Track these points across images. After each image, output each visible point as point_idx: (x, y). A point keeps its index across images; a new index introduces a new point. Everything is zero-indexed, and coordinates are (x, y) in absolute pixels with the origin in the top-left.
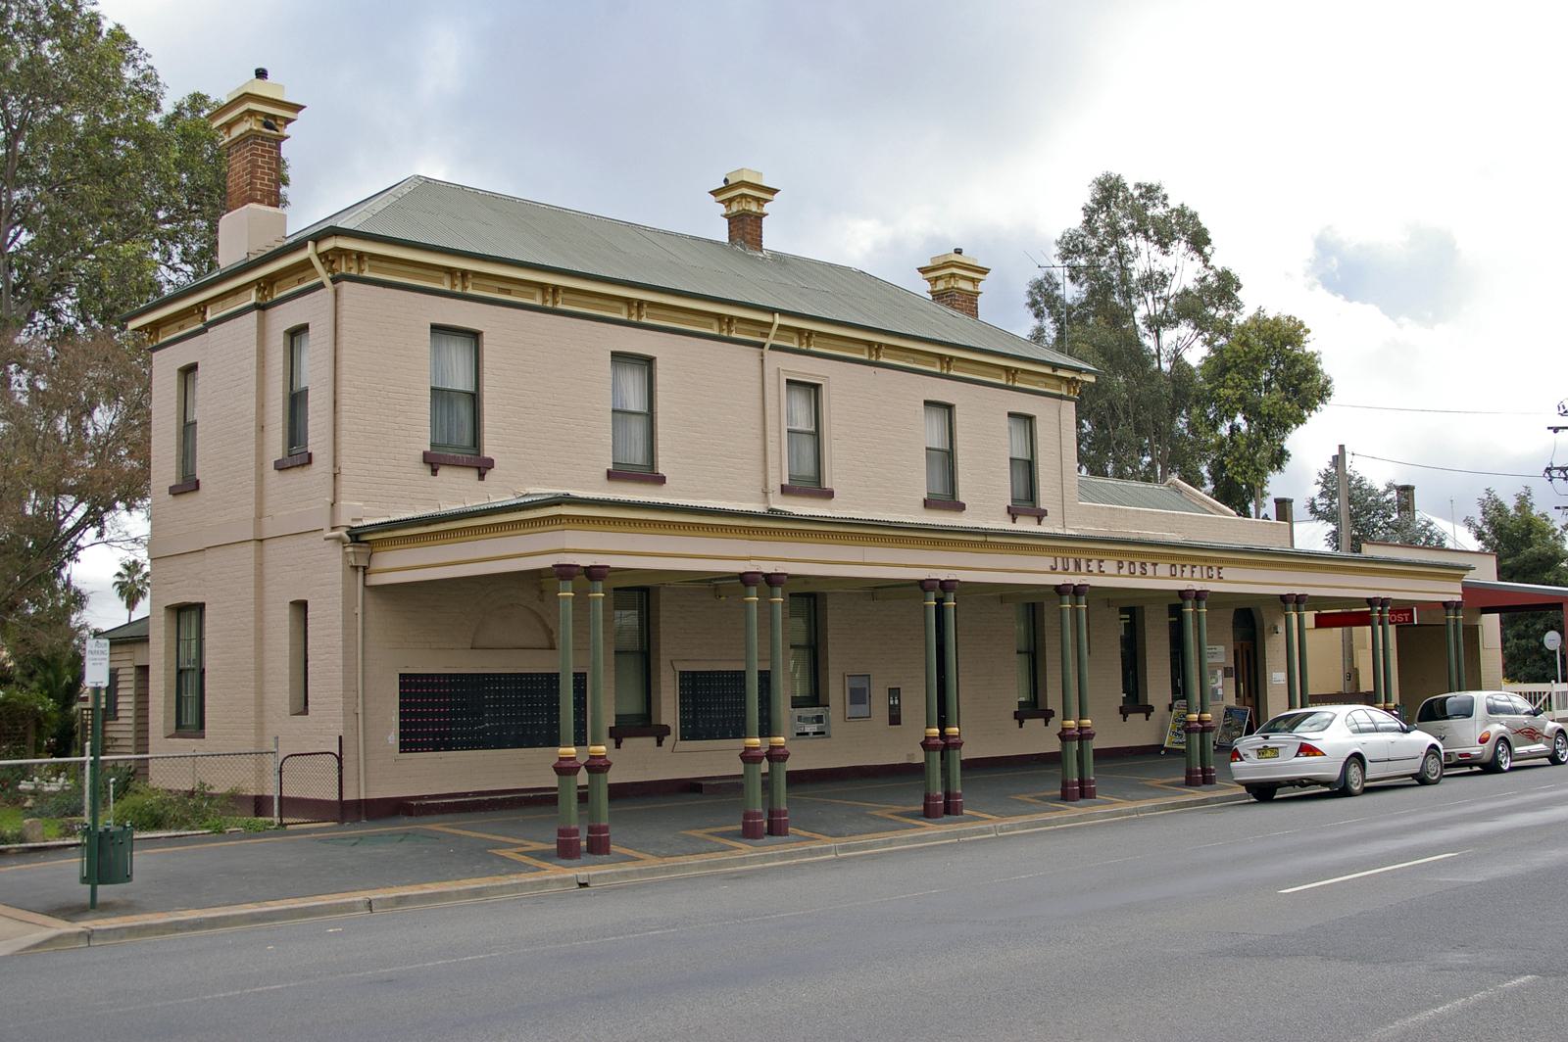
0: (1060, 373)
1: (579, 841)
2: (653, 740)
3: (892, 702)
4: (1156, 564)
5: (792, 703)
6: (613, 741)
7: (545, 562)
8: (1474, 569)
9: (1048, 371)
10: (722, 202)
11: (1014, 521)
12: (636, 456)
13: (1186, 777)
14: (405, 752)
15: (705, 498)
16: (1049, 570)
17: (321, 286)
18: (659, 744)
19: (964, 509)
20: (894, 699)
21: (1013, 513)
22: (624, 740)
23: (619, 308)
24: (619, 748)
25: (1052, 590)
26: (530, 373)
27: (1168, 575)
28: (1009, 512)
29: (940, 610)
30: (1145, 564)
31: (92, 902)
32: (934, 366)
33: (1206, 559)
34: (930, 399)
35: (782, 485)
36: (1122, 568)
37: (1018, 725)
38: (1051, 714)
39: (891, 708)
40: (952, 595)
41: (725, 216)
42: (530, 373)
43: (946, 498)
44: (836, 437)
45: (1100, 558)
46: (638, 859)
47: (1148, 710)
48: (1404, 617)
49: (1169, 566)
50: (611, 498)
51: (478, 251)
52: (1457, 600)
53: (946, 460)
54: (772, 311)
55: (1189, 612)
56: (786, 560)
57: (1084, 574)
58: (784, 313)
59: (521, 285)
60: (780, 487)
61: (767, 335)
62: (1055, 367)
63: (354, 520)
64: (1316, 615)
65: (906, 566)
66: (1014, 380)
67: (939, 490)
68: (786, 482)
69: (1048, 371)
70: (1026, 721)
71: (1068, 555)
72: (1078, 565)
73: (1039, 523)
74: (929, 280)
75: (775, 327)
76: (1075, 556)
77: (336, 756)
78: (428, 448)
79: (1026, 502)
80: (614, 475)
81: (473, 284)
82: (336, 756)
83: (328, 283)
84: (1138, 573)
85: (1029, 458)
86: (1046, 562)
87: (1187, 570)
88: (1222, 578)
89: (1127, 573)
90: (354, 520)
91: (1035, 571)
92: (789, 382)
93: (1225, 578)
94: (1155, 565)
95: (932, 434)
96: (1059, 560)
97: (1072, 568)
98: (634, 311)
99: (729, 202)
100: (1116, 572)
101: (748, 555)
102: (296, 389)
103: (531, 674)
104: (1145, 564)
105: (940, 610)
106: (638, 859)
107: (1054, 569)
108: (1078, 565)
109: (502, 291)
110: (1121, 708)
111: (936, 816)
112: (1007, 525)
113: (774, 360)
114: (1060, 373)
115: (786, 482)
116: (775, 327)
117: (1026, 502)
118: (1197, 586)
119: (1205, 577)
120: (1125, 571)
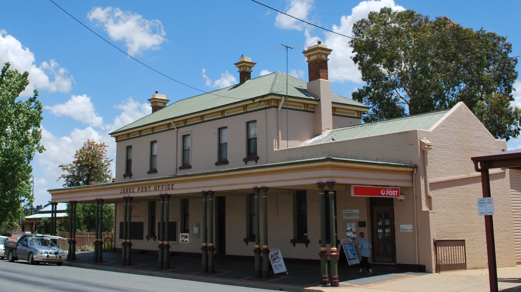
9: (251, 102)
10: (238, 67)
11: (246, 164)
17: (174, 129)
27: (154, 190)
31: (102, 253)
33: (167, 182)
41: (239, 71)
43: (222, 161)
45: (133, 187)
47: (307, 242)
48: (395, 193)
49: (154, 187)
69: (251, 102)
73: (256, 162)
74: (307, 56)
83: (175, 128)
84: (144, 190)
86: (119, 191)
87: (160, 188)
91: (152, 192)
94: (149, 187)
99: (240, 67)
107: (121, 193)
118: (163, 193)
119: (167, 188)
120: (140, 191)
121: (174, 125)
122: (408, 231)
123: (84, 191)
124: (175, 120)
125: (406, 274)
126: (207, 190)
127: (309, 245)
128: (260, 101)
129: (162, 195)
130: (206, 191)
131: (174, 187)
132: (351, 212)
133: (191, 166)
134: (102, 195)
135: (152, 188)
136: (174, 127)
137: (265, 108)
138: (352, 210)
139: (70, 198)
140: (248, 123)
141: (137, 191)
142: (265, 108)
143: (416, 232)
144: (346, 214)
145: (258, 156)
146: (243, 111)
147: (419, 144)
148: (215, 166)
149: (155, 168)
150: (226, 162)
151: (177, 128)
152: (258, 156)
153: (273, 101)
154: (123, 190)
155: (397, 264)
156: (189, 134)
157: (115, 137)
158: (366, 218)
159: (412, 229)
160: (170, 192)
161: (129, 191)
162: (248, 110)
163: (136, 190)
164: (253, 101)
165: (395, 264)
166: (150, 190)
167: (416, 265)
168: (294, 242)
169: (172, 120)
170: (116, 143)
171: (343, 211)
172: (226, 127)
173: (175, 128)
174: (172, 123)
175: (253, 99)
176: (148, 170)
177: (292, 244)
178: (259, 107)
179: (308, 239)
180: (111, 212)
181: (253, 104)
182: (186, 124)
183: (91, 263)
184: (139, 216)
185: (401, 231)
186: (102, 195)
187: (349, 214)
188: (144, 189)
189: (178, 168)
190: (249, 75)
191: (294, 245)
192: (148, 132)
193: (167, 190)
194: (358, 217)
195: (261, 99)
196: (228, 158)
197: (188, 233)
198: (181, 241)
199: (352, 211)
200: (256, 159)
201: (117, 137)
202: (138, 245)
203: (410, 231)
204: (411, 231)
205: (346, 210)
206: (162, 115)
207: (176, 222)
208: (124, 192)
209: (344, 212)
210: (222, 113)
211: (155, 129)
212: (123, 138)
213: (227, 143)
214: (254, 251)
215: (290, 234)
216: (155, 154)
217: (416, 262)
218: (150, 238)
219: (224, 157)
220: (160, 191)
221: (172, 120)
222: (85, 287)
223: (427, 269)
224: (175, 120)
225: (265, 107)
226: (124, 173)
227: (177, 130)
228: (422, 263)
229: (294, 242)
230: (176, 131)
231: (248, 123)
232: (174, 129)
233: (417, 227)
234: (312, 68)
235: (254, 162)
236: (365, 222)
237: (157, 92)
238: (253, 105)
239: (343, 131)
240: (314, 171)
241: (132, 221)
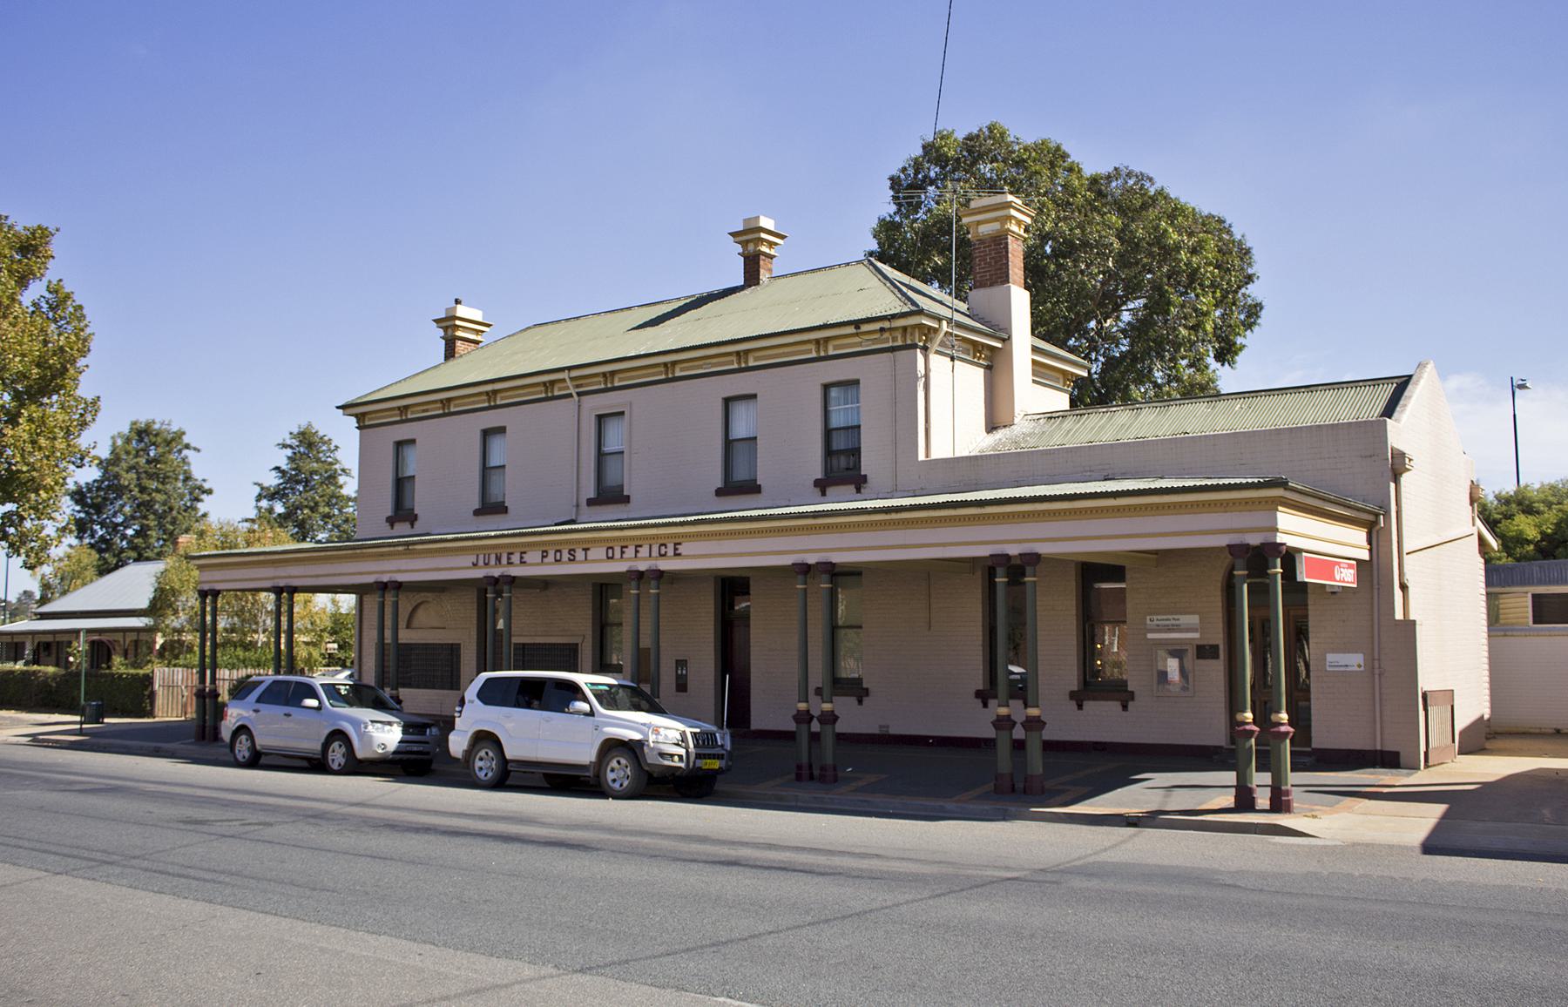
0: (865, 328)
3: (679, 672)
4: (588, 549)
7: (787, 560)
9: (851, 330)
13: (1271, 800)
16: (471, 565)
17: (570, 396)
19: (629, 502)
20: (682, 669)
24: (867, 692)
30: (574, 550)
36: (546, 557)
39: (678, 677)
49: (605, 549)
50: (1099, 491)
55: (1276, 573)
57: (504, 566)
71: (478, 552)
72: (498, 559)
73: (412, 526)
76: (496, 551)
83: (574, 395)
86: (469, 559)
87: (630, 552)
93: (528, 562)
94: (586, 550)
96: (481, 557)
97: (493, 561)
102: (400, 476)
103: (545, 644)
104: (574, 550)
107: (475, 565)
108: (498, 559)
120: (551, 558)
121: (571, 387)
122: (1349, 669)
123: (1294, 491)
124: (575, 373)
125: (1358, 773)
126: (385, 578)
127: (866, 700)
128: (882, 330)
129: (382, 582)
130: (496, 575)
131: (681, 549)
132: (1174, 622)
133: (628, 497)
134: (399, 571)
135: (598, 553)
136: (573, 391)
137: (892, 349)
138: (1176, 617)
139: (273, 578)
140: (727, 401)
141: (634, 556)
142: (892, 349)
143: (1377, 671)
144: (1158, 625)
145: (862, 473)
146: (486, 405)
147: (1390, 455)
148: (716, 498)
149: (500, 499)
150: (501, 509)
151: (579, 394)
152: (862, 473)
153: (917, 330)
154: (481, 557)
155: (1313, 749)
156: (622, 410)
157: (356, 416)
158: (1221, 636)
159: (1362, 664)
160: (665, 565)
161: (504, 561)
162: (498, 402)
163: (533, 556)
164: (855, 328)
165: (1309, 749)
166: (589, 558)
167: (1376, 751)
169: (566, 371)
170: (358, 431)
171: (1148, 618)
172: (413, 441)
173: (574, 395)
174: (568, 380)
175: (857, 323)
176: (719, 483)
177: (979, 702)
178: (868, 346)
179: (865, 686)
181: (857, 335)
182: (404, 418)
183: (190, 741)
184: (444, 628)
185: (1328, 669)
186: (399, 571)
187: (1168, 626)
188: (566, 556)
189: (583, 503)
190: (747, 275)
192: (478, 402)
193: (656, 558)
194: (1196, 635)
195: (886, 325)
196: (506, 500)
199: (1178, 620)
200: (858, 482)
201: (360, 417)
203: (1357, 669)
204: (1358, 669)
206: (470, 369)
207: (577, 644)
208: (486, 564)
209: (1148, 622)
210: (402, 412)
211: (499, 396)
212: (473, 403)
213: (414, 477)
214: (994, 724)
216: (409, 473)
217: (1375, 745)
218: (1089, 699)
219: (407, 505)
220: (630, 559)
221: (566, 371)
223: (1402, 760)
224: (575, 373)
225: (892, 347)
226: (389, 513)
227: (579, 401)
228: (1390, 747)
230: (577, 404)
231: (727, 401)
232: (570, 396)
233: (1379, 660)
234: (986, 255)
235: (407, 525)
236: (1217, 646)
237: (457, 302)
238: (857, 340)
239: (1062, 423)
240: (1037, 522)
241: (400, 642)
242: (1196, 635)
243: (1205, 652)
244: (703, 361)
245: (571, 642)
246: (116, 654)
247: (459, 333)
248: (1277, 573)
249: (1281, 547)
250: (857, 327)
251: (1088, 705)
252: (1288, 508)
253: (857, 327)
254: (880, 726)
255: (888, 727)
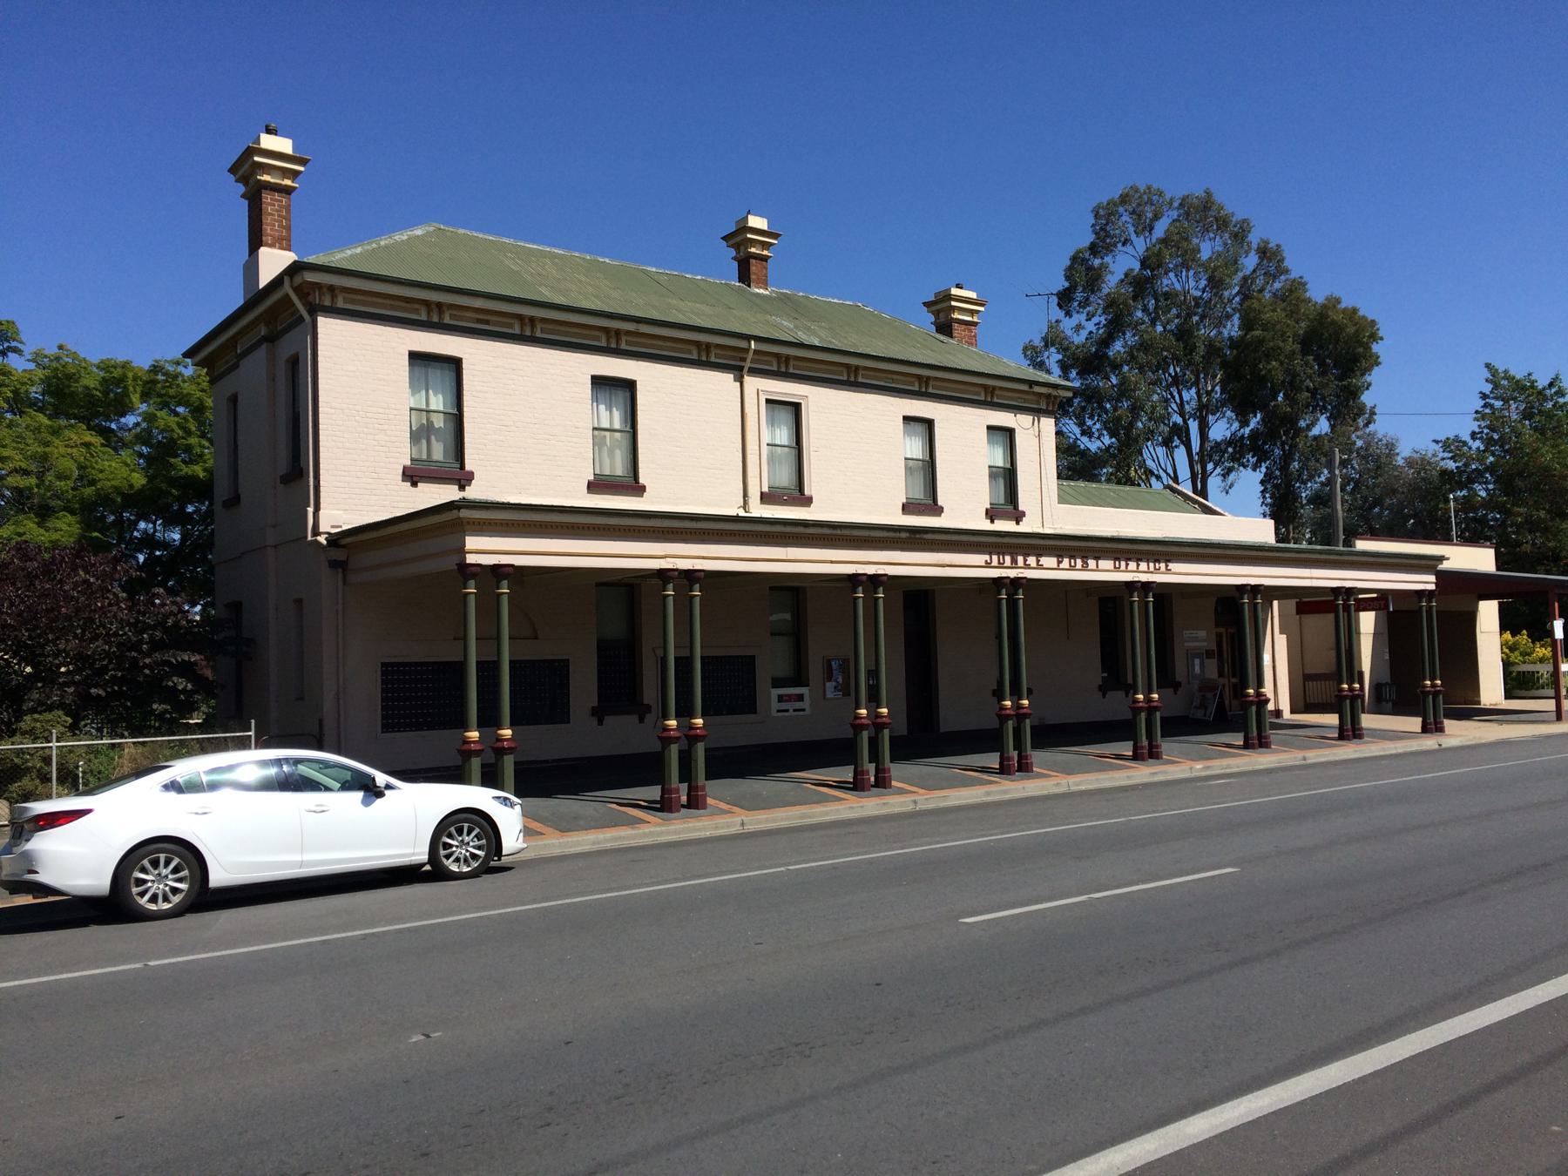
0: (1037, 389)
1: (869, 779)
2: (635, 718)
5: (772, 683)
6: (1101, 693)
8: (1448, 559)
9: (1025, 387)
11: (992, 522)
12: (619, 468)
13: (1133, 752)
14: (387, 732)
15: (686, 504)
18: (641, 720)
21: (991, 515)
22: (606, 717)
23: (417, 309)
24: (643, 722)
25: (991, 581)
26: (510, 395)
27: (1112, 568)
28: (987, 514)
29: (1012, 604)
32: (913, 386)
34: (909, 414)
35: (762, 493)
37: (1124, 695)
38: (648, 709)
40: (698, 585)
42: (510, 395)
44: (816, 449)
46: (844, 799)
51: (354, 269)
52: (1430, 588)
53: (928, 469)
54: (748, 338)
56: (704, 558)
58: (758, 339)
59: (377, 297)
60: (759, 494)
61: (744, 360)
62: (1031, 383)
63: (333, 527)
64: (1297, 603)
65: (832, 562)
66: (992, 397)
67: (919, 494)
68: (765, 489)
69: (1025, 387)
70: (606, 717)
72: (1014, 561)
73: (1018, 523)
75: (751, 353)
77: (314, 736)
78: (408, 463)
79: (1008, 501)
80: (595, 486)
81: (344, 299)
82: (314, 736)
85: (1008, 466)
86: (980, 559)
88: (1170, 570)
89: (1068, 567)
90: (333, 527)
92: (768, 401)
95: (915, 448)
98: (924, 385)
100: (1056, 566)
101: (663, 554)
105: (1012, 604)
106: (844, 799)
109: (479, 321)
110: (1100, 686)
111: (1143, 760)
112: (986, 525)
113: (752, 383)
114: (1037, 389)
115: (765, 489)
116: (751, 353)
117: (1008, 501)
166: (1100, 568)
168: (1104, 689)
177: (595, 721)
180: (50, 525)
191: (600, 722)
194: (1205, 644)
197: (808, 686)
198: (775, 714)
202: (102, 783)
205: (1187, 632)
215: (1096, 675)
222: (863, 675)
229: (1104, 689)
242: (1205, 644)
243: (1209, 654)
244: (885, 375)
245: (711, 655)
246: (1561, 640)
247: (956, 316)
248: (1135, 601)
249: (1152, 585)
250: (1031, 387)
251: (609, 720)
252: (1306, 567)
253: (1031, 387)
254: (1040, 719)
255: (1044, 719)
